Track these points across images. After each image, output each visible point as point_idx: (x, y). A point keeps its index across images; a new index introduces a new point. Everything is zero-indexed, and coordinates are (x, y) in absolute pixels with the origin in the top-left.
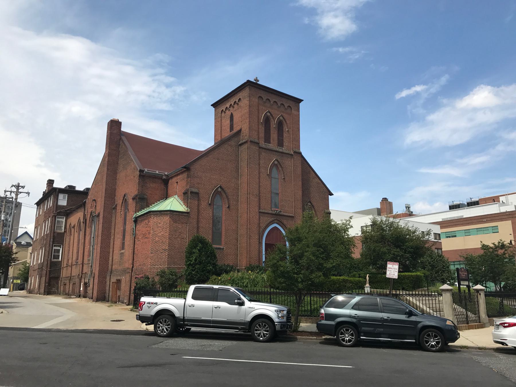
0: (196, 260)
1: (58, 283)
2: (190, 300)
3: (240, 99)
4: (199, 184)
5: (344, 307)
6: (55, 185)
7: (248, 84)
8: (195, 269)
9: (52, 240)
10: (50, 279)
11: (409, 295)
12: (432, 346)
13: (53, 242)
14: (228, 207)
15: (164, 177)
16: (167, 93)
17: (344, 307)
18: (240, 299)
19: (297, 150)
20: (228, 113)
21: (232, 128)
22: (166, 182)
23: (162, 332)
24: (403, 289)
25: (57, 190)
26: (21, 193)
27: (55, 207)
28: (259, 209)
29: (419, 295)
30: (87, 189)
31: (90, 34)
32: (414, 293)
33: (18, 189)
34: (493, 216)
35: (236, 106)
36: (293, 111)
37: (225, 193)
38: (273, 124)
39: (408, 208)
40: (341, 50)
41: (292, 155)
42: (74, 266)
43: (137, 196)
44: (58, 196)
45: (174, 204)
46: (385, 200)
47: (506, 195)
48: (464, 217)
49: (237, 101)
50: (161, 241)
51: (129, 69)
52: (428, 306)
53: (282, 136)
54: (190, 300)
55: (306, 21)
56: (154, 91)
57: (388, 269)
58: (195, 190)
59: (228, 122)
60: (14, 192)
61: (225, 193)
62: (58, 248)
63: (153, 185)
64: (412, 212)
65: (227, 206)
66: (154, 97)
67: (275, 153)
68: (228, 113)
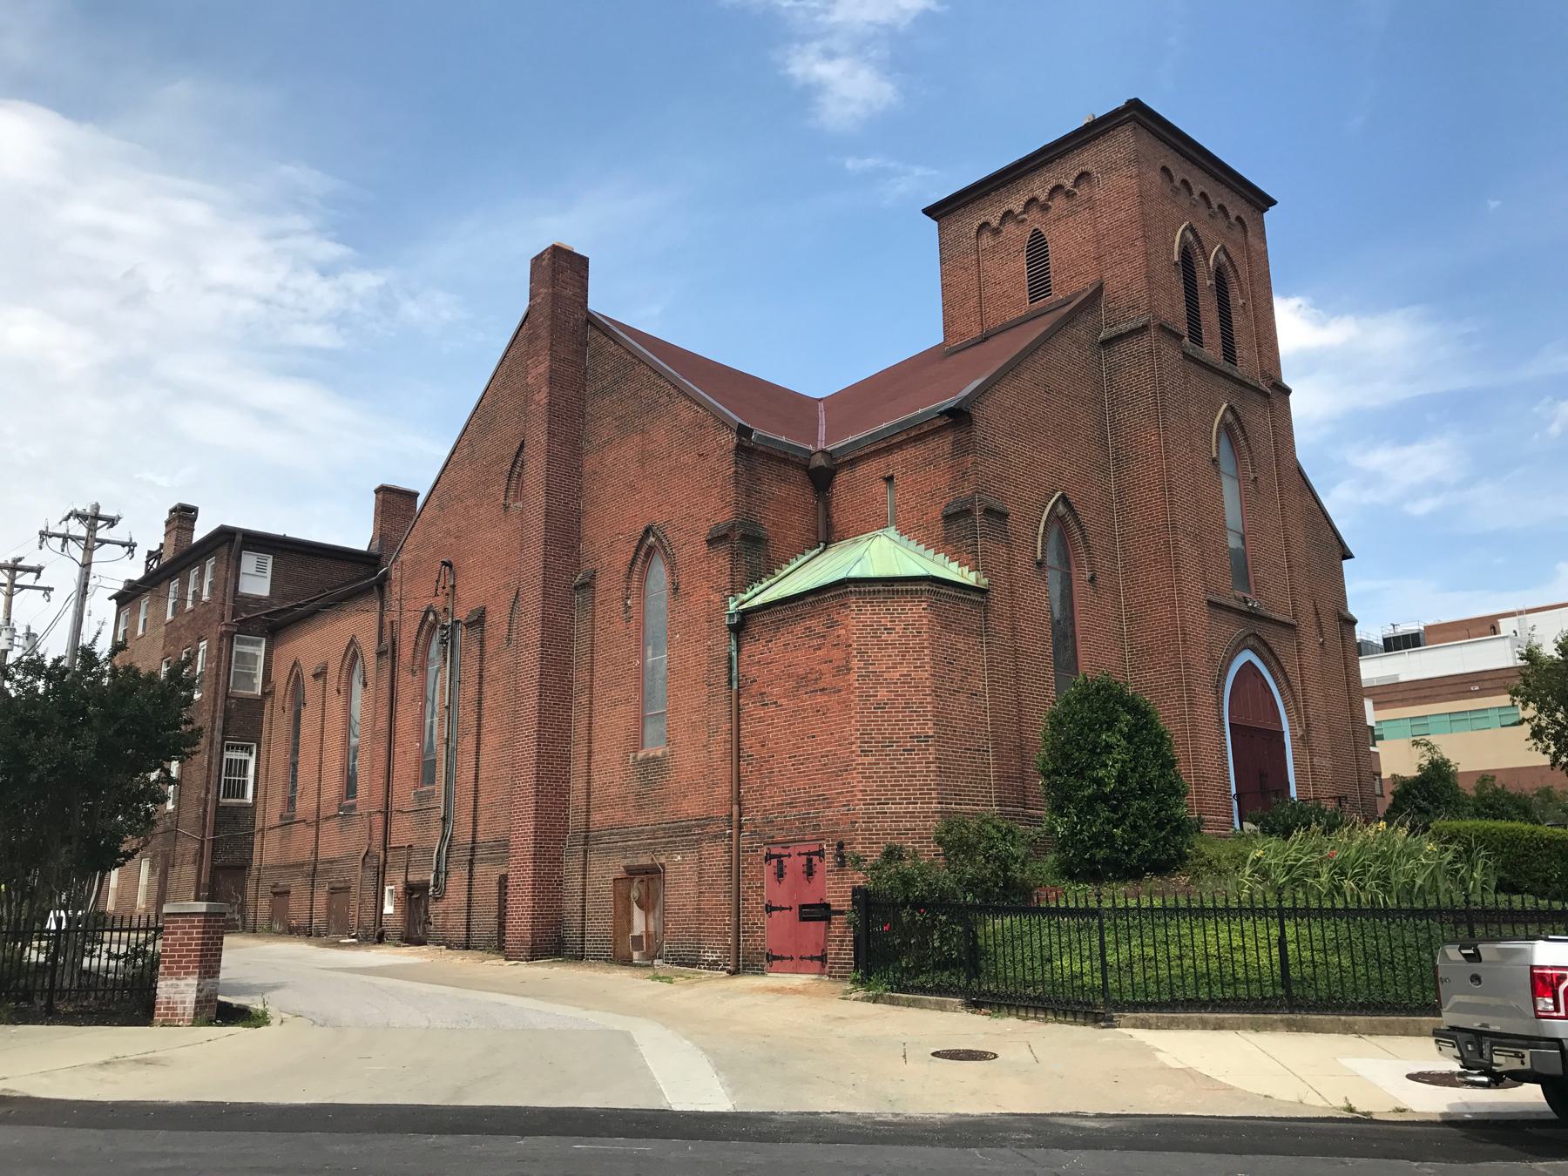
0: (1122, 779)
1: (242, 890)
3: (1084, 176)
7: (1135, 105)
8: (1125, 816)
9: (219, 723)
10: (215, 869)
13: (225, 732)
14: (1092, 579)
15: (819, 461)
16: (324, 295)
21: (1039, 284)
25: (239, 538)
26: (103, 542)
27: (229, 603)
33: (92, 529)
34: (1505, 674)
41: (1267, 395)
42: (334, 823)
43: (732, 528)
44: (239, 559)
47: (1521, 613)
48: (1402, 679)
50: (901, 702)
51: (194, 213)
56: (281, 287)
60: (76, 539)
63: (779, 490)
65: (1088, 575)
66: (281, 306)
68: (1016, 235)
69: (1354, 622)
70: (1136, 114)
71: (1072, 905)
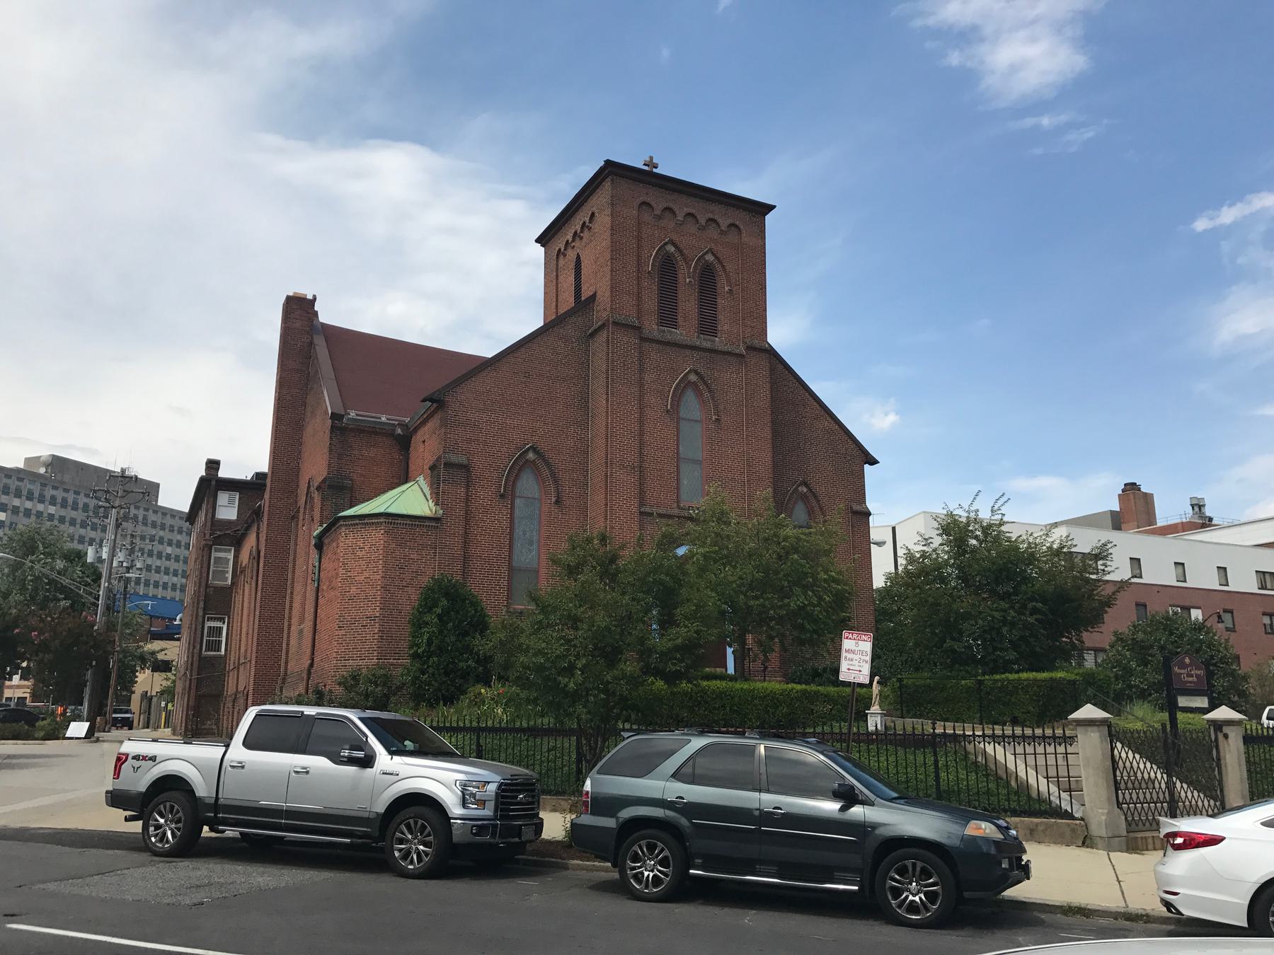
1: (217, 711)
2: (238, 752)
3: (593, 214)
4: (469, 441)
5: (666, 775)
6: (223, 473)
9: (202, 605)
10: (199, 698)
11: (994, 738)
12: (913, 908)
14: (557, 502)
17: (666, 775)
18: (361, 745)
19: (756, 343)
20: (572, 255)
22: (404, 442)
23: (161, 841)
24: (1015, 722)
28: (642, 504)
29: (1054, 737)
30: (257, 474)
31: (419, 138)
32: (1049, 732)
35: (586, 234)
36: (745, 239)
37: (548, 465)
38: (686, 277)
39: (1198, 506)
40: (1046, 121)
41: (742, 356)
45: (412, 499)
46: (1131, 488)
49: (587, 220)
50: (363, 596)
52: (1042, 769)
53: (714, 305)
54: (238, 752)
55: (954, 59)
57: (844, 654)
58: (462, 460)
59: (572, 278)
61: (548, 465)
62: (218, 624)
64: (1211, 519)
67: (688, 352)
68: (572, 255)
69: (869, 514)
70: (611, 170)
71: (468, 724)
